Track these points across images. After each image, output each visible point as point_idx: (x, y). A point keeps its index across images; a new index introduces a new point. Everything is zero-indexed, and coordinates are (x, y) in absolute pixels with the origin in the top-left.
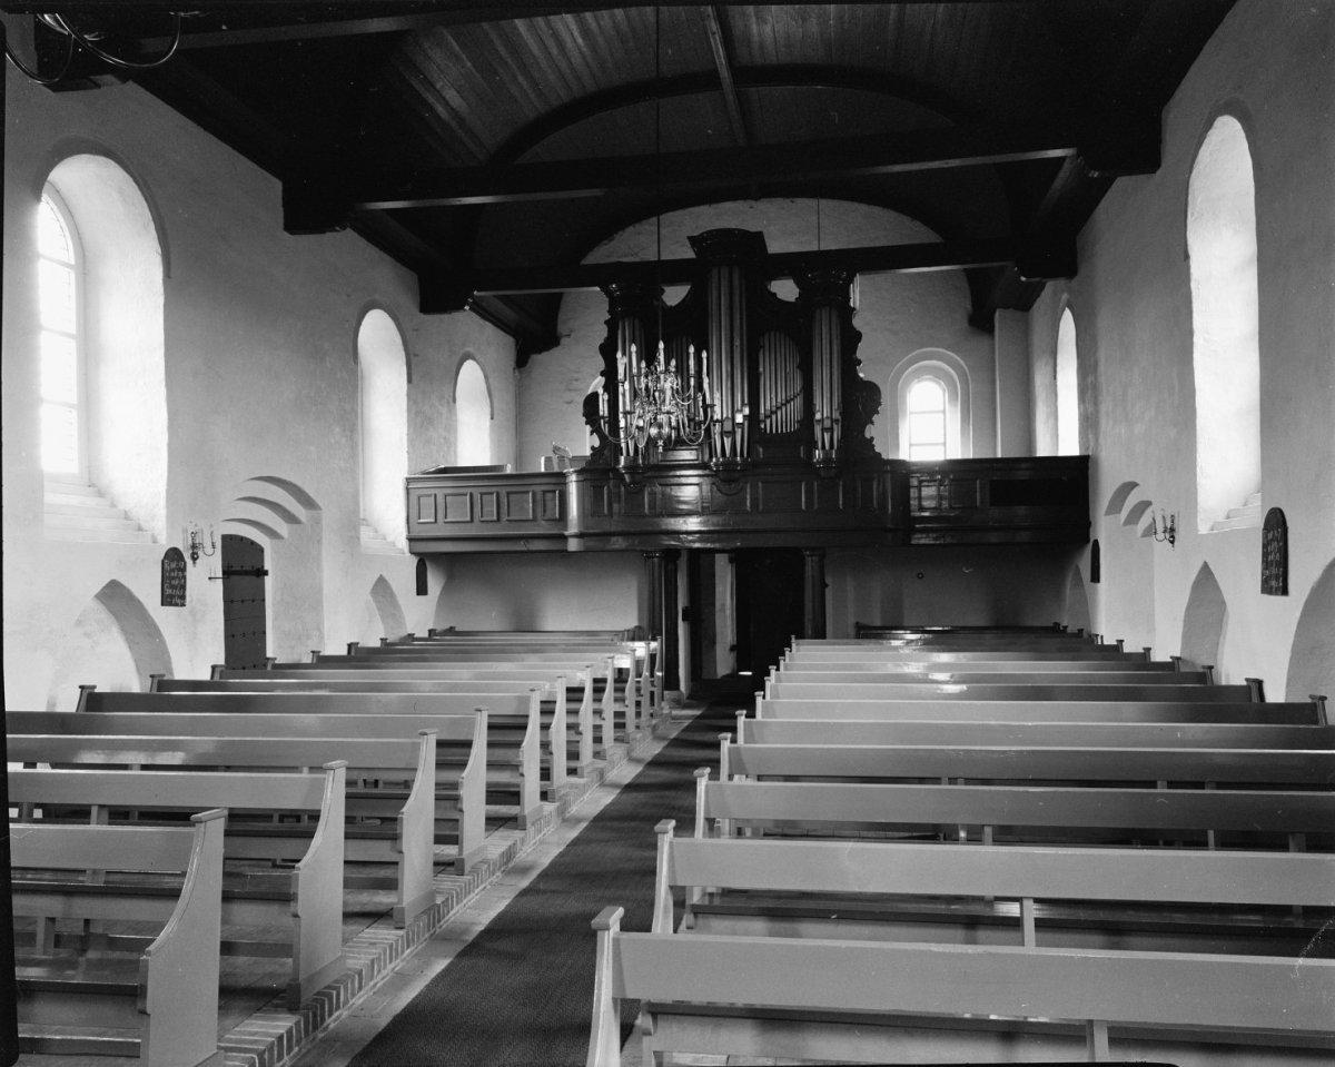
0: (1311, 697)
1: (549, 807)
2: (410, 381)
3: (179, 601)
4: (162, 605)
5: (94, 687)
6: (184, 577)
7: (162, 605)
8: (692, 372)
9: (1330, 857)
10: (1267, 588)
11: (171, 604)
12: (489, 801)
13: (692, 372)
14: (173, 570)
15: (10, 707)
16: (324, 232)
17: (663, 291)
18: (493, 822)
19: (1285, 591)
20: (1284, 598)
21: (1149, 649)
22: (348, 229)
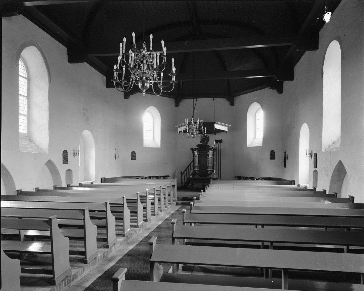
0: (334, 192)
1: (121, 239)
2: (50, 81)
3: (66, 162)
4: (63, 164)
5: (22, 190)
6: (68, 156)
7: (63, 164)
8: (203, 132)
9: (363, 255)
10: (271, 159)
11: (65, 164)
12: (70, 254)
13: (203, 132)
14: (65, 155)
15: (2, 194)
16: (79, 63)
17: (351, 286)
18: (117, 235)
19: (274, 159)
20: (131, 159)
21: (336, 193)
22: (208, 144)
